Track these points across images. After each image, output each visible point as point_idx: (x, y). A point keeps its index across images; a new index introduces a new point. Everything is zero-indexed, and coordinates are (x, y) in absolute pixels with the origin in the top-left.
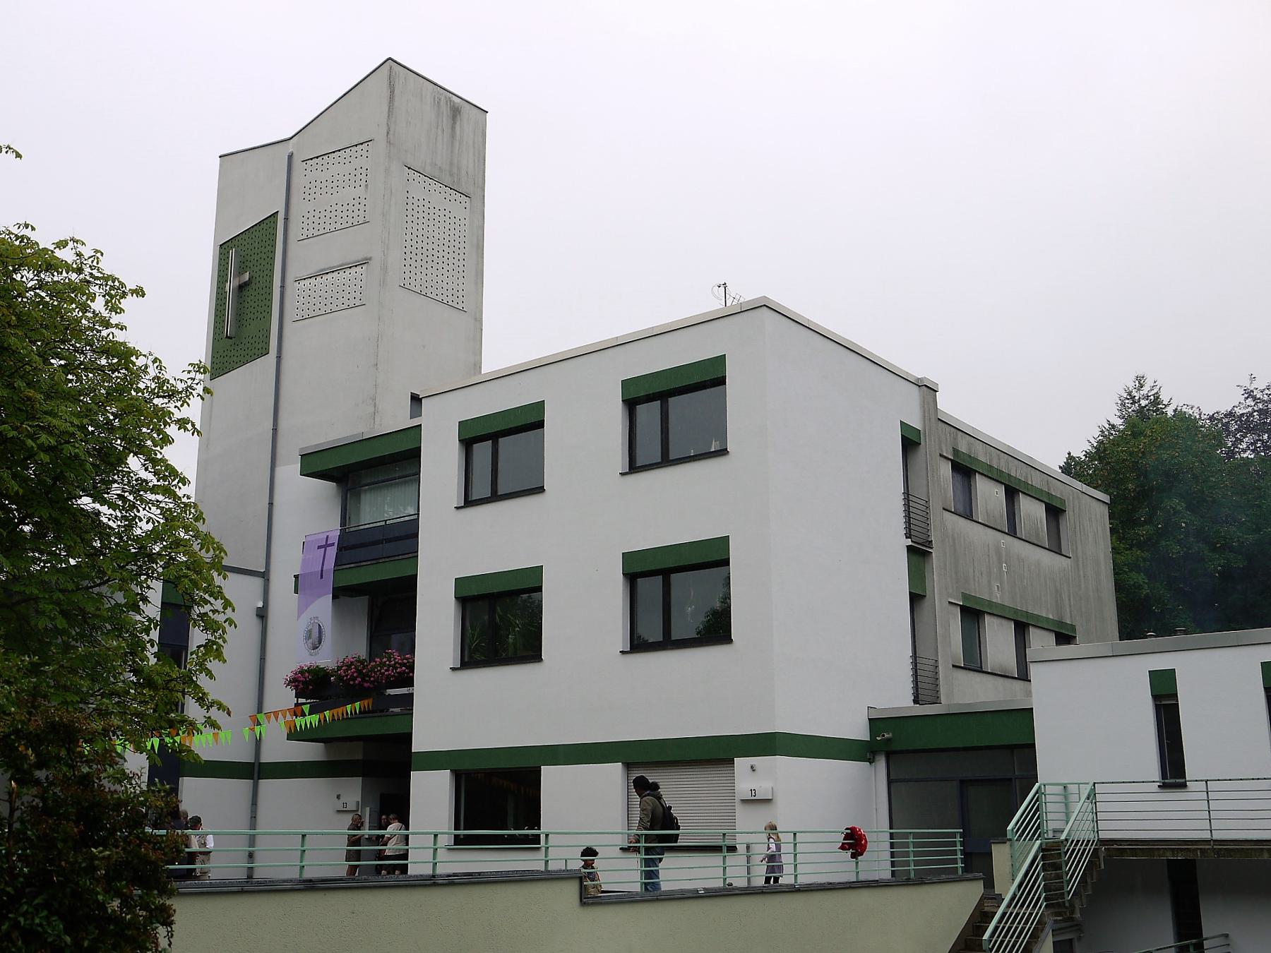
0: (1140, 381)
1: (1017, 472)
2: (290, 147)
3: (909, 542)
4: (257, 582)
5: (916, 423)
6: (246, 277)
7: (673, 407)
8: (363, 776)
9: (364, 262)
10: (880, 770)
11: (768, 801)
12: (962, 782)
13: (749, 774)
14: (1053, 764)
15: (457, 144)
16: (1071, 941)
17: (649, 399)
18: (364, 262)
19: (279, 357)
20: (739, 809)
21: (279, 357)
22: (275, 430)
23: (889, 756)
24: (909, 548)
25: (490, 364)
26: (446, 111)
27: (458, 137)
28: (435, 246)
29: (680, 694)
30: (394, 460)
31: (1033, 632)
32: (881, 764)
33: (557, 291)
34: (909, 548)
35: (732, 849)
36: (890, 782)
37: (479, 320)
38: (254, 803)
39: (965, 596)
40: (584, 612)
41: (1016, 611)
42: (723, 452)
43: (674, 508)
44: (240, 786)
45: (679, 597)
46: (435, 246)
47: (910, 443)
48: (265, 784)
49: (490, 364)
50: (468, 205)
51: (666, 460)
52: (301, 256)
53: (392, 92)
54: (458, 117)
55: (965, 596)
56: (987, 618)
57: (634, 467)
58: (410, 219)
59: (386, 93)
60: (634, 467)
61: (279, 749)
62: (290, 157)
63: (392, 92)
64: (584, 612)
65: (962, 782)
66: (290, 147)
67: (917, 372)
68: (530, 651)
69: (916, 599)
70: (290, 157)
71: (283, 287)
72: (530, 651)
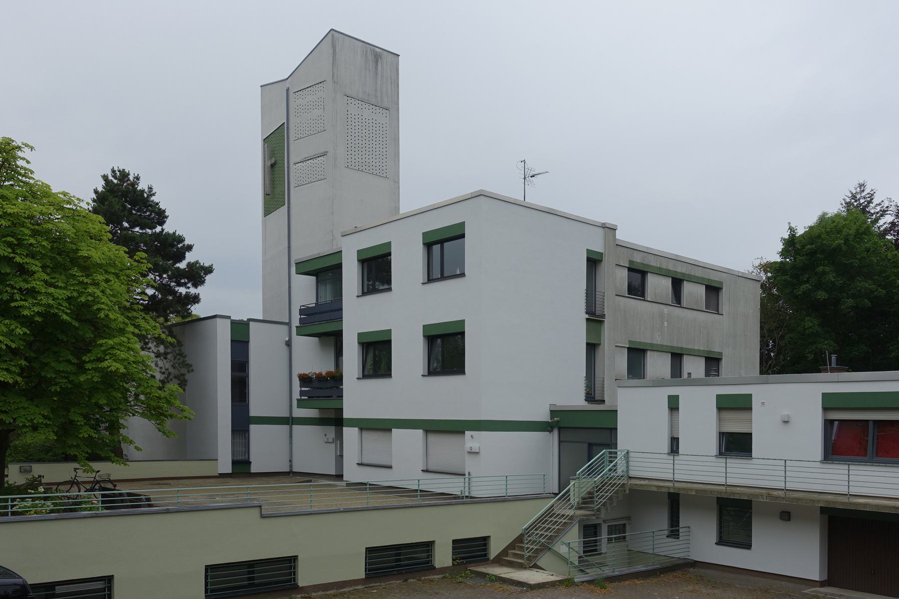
0: (862, 186)
1: (680, 269)
2: (287, 84)
3: (587, 316)
4: (286, 328)
5: (598, 248)
6: (273, 161)
7: (444, 250)
8: (342, 426)
9: (324, 154)
10: (553, 438)
11: (478, 453)
12: (590, 444)
13: (473, 440)
14: (624, 440)
15: (379, 78)
16: (624, 525)
17: (436, 243)
18: (324, 154)
19: (289, 207)
20: (467, 456)
21: (289, 207)
22: (289, 247)
23: (560, 429)
24: (587, 319)
25: (404, 209)
26: (371, 57)
27: (380, 73)
28: (367, 142)
29: (445, 398)
30: (326, 272)
31: (686, 359)
32: (556, 433)
33: (432, 169)
34: (587, 319)
35: (464, 475)
36: (560, 442)
37: (397, 182)
38: (291, 436)
39: (630, 342)
40: (409, 354)
41: (672, 347)
42: (462, 275)
43: (443, 304)
44: (286, 428)
45: (446, 350)
46: (367, 142)
47: (593, 262)
48: (296, 428)
49: (404, 209)
50: (388, 115)
51: (443, 278)
52: (297, 150)
53: (334, 50)
54: (380, 62)
55: (630, 342)
56: (649, 353)
57: (430, 280)
58: (349, 127)
59: (331, 51)
60: (430, 280)
61: (299, 413)
62: (288, 90)
63: (334, 50)
64: (409, 354)
65: (590, 444)
66: (287, 84)
67: (602, 220)
68: (387, 373)
69: (592, 348)
70: (288, 90)
71: (288, 167)
72: (387, 373)
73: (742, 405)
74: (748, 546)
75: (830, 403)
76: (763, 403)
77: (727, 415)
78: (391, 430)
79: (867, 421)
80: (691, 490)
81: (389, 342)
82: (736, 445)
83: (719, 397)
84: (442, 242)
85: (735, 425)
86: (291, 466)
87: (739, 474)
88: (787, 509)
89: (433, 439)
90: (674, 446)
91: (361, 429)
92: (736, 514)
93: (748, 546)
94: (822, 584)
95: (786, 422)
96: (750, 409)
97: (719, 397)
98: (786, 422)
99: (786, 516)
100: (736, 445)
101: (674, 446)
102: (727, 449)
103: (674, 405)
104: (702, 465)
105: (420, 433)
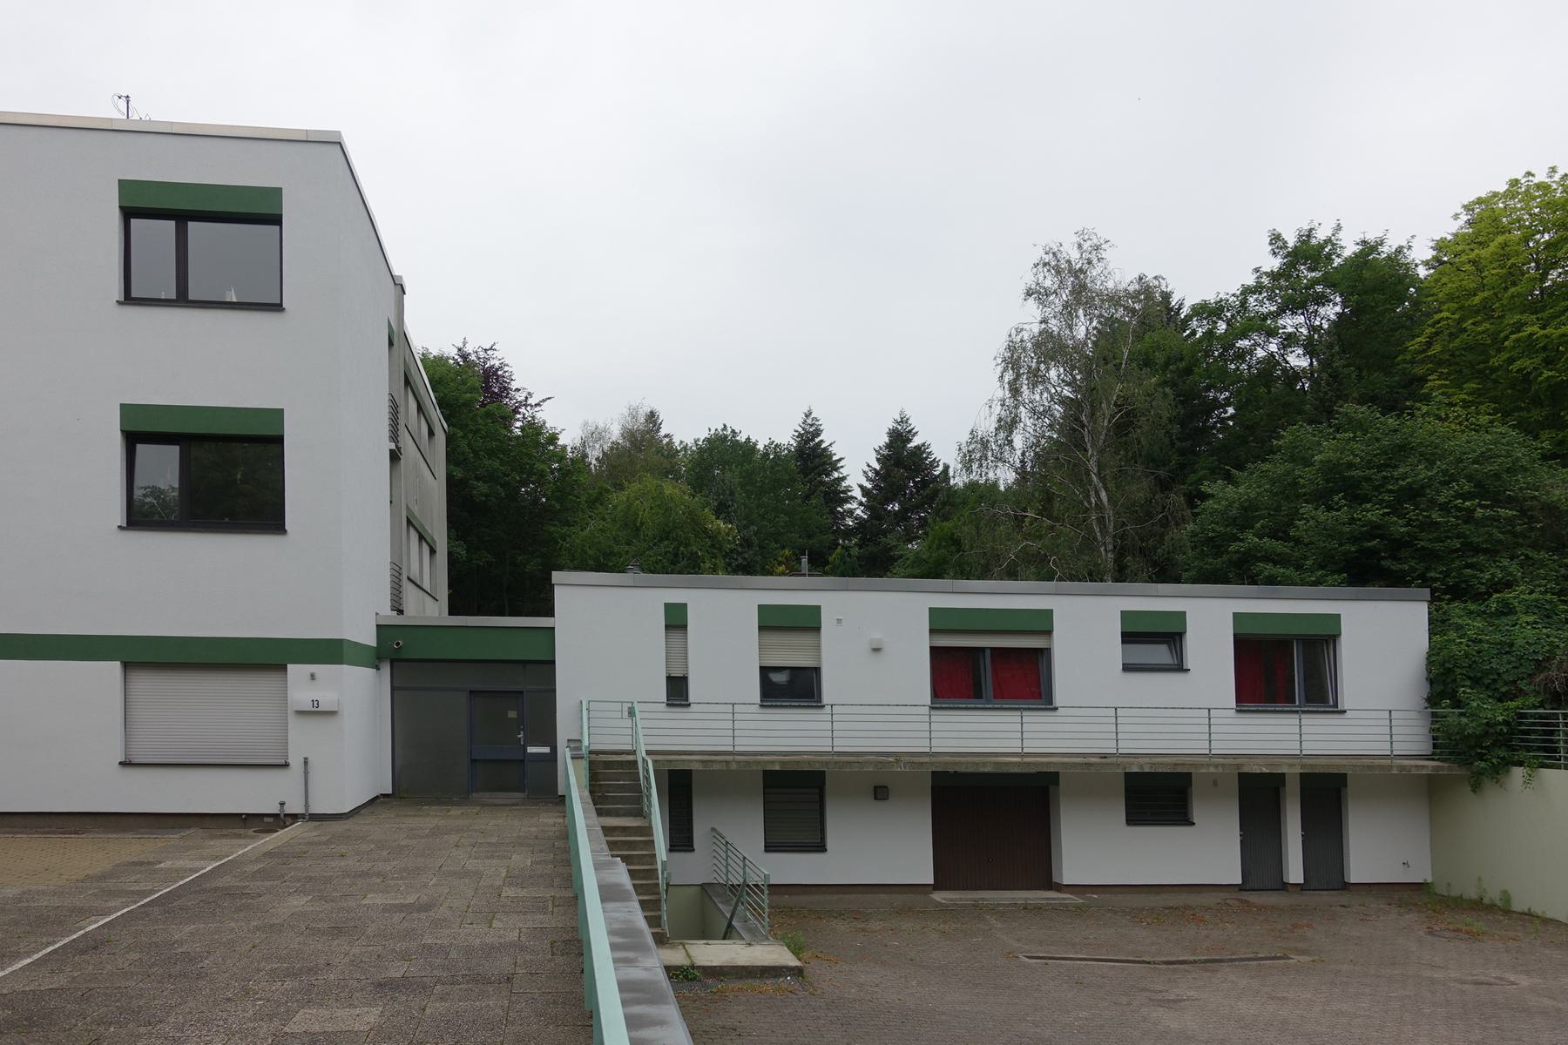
11: (333, 713)
20: (294, 724)
23: (392, 662)
32: (386, 670)
73: (806, 622)
74: (821, 847)
75: (940, 622)
76: (839, 621)
77: (774, 638)
78: (283, 668)
79: (983, 649)
80: (773, 762)
81: (276, 441)
82: (792, 687)
83: (933, 612)
84: (182, 218)
85: (790, 653)
86: (307, 805)
87: (791, 734)
88: (879, 782)
89: (145, 683)
90: (677, 689)
91: (126, 666)
92: (796, 798)
93: (821, 847)
94: (939, 885)
95: (877, 650)
96: (818, 629)
97: (933, 612)
98: (877, 650)
99: (880, 793)
100: (792, 687)
101: (677, 689)
102: (1324, 700)
103: (676, 620)
104: (729, 719)
105: (112, 669)
